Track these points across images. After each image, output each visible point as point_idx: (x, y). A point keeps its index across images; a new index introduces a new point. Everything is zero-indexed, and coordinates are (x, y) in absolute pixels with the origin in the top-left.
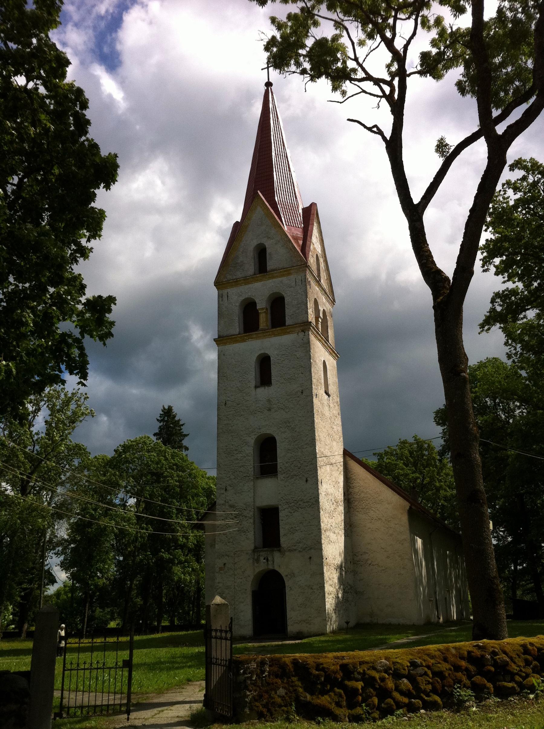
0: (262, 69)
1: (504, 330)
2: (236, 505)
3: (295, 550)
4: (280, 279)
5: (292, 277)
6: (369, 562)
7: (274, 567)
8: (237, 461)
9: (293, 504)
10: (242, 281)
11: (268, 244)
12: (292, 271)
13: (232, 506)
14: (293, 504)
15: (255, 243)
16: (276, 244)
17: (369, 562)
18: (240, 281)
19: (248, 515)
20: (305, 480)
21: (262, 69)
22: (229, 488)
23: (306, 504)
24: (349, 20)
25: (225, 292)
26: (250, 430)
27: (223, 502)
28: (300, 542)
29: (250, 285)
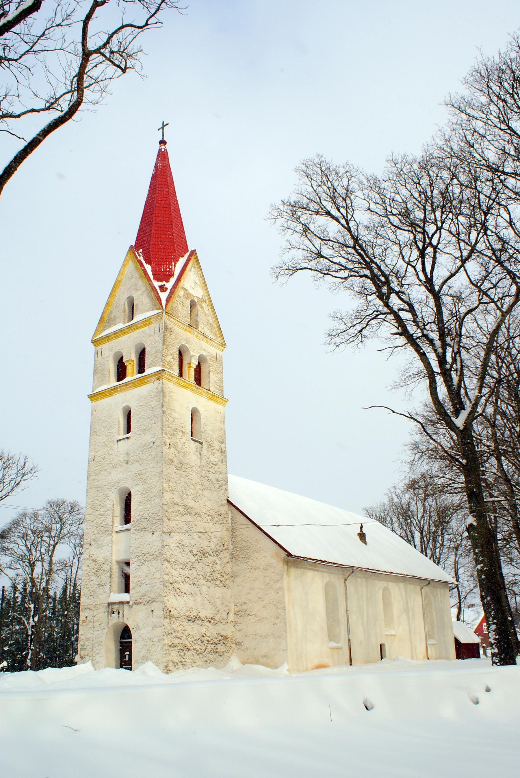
0: (158, 130)
1: (458, 428)
2: (98, 559)
3: (141, 603)
4: (142, 329)
5: (152, 326)
6: (248, 612)
7: (123, 620)
8: (100, 516)
9: (141, 557)
10: (113, 336)
11: (136, 296)
12: (152, 320)
13: (94, 561)
14: (141, 557)
15: (126, 296)
16: (142, 295)
17: (248, 612)
18: (111, 335)
19: (105, 569)
20: (152, 533)
21: (158, 130)
22: (93, 543)
23: (152, 557)
24: (434, 258)
25: (100, 347)
26: (112, 484)
27: (88, 557)
28: (145, 596)
29: (120, 339)
